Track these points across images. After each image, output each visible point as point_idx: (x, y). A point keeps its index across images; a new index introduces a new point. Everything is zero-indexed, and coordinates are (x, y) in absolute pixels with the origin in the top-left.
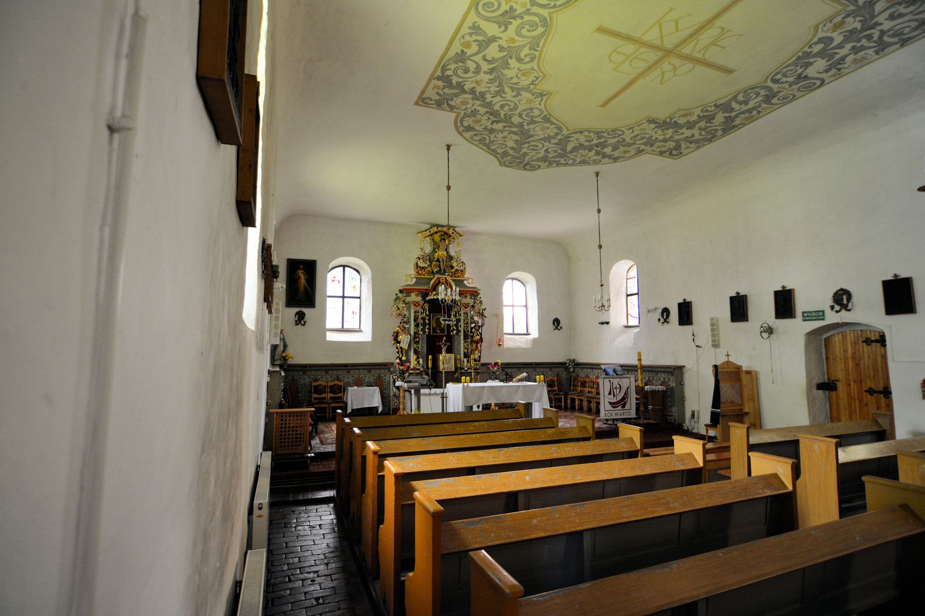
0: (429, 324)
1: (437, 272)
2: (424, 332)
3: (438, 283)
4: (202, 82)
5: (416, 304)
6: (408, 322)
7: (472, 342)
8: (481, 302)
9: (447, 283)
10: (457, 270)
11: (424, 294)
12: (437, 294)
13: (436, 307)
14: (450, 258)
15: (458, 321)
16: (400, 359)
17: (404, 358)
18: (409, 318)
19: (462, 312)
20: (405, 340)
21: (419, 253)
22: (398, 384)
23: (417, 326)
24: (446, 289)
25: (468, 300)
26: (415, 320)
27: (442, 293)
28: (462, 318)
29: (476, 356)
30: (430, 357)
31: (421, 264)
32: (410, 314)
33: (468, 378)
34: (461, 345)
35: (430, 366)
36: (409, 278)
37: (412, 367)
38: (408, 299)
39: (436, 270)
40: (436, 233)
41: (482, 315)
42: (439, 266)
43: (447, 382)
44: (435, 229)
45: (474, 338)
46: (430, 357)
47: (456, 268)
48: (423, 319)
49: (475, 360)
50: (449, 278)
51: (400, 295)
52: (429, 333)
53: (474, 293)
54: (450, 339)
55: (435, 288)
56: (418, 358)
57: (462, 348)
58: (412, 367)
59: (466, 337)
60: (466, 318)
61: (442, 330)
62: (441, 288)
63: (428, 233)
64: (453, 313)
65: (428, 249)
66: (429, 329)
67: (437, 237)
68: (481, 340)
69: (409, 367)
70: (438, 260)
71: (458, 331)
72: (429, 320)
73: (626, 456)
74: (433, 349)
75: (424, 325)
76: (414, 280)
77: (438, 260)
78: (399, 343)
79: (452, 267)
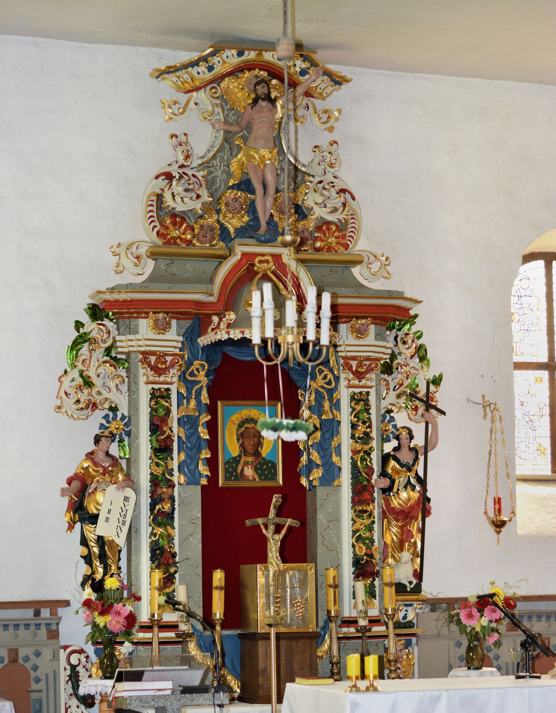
0: (213, 445)
1: (242, 232)
2: (193, 479)
3: (247, 275)
4: (306, 303)
5: (157, 364)
6: (128, 432)
7: (389, 512)
8: (421, 354)
9: (279, 275)
10: (323, 225)
11: (197, 319)
12: (245, 321)
13: (238, 375)
14: (297, 175)
15: (330, 428)
16: (98, 587)
17: (111, 583)
18: (129, 421)
19: (344, 394)
20: (117, 508)
21: (167, 157)
22: (88, 686)
23: (162, 450)
24: (279, 304)
25: (370, 343)
26: (156, 427)
27: (260, 318)
28: (345, 417)
29: (404, 573)
30: (218, 576)
31: (181, 202)
32: (133, 405)
33: (372, 662)
34: (337, 517)
35: (218, 611)
36: (127, 262)
37: (144, 617)
38: (126, 343)
39: (233, 223)
40: (234, 73)
41: (425, 403)
42: (252, 209)
43: (287, 676)
44: (230, 58)
45: (396, 494)
46: (218, 576)
47: (319, 212)
48: (188, 422)
49: (400, 588)
50: (288, 257)
51: (90, 326)
52: (213, 478)
53: (393, 315)
54: (297, 502)
55: (233, 296)
56: (168, 580)
57: (347, 540)
58: (144, 617)
59: (361, 493)
60: (361, 416)
61: (265, 468)
62: (260, 299)
63: (202, 73)
64: (307, 399)
65: (204, 139)
66: (212, 463)
67: (238, 89)
68: (424, 505)
69: (131, 619)
70: (245, 185)
71: (331, 473)
72: (212, 426)
73: (318, 322)
74: (230, 541)
75: (191, 447)
76: (149, 266)
77: (245, 185)
78: (94, 519)
79: (301, 212)
